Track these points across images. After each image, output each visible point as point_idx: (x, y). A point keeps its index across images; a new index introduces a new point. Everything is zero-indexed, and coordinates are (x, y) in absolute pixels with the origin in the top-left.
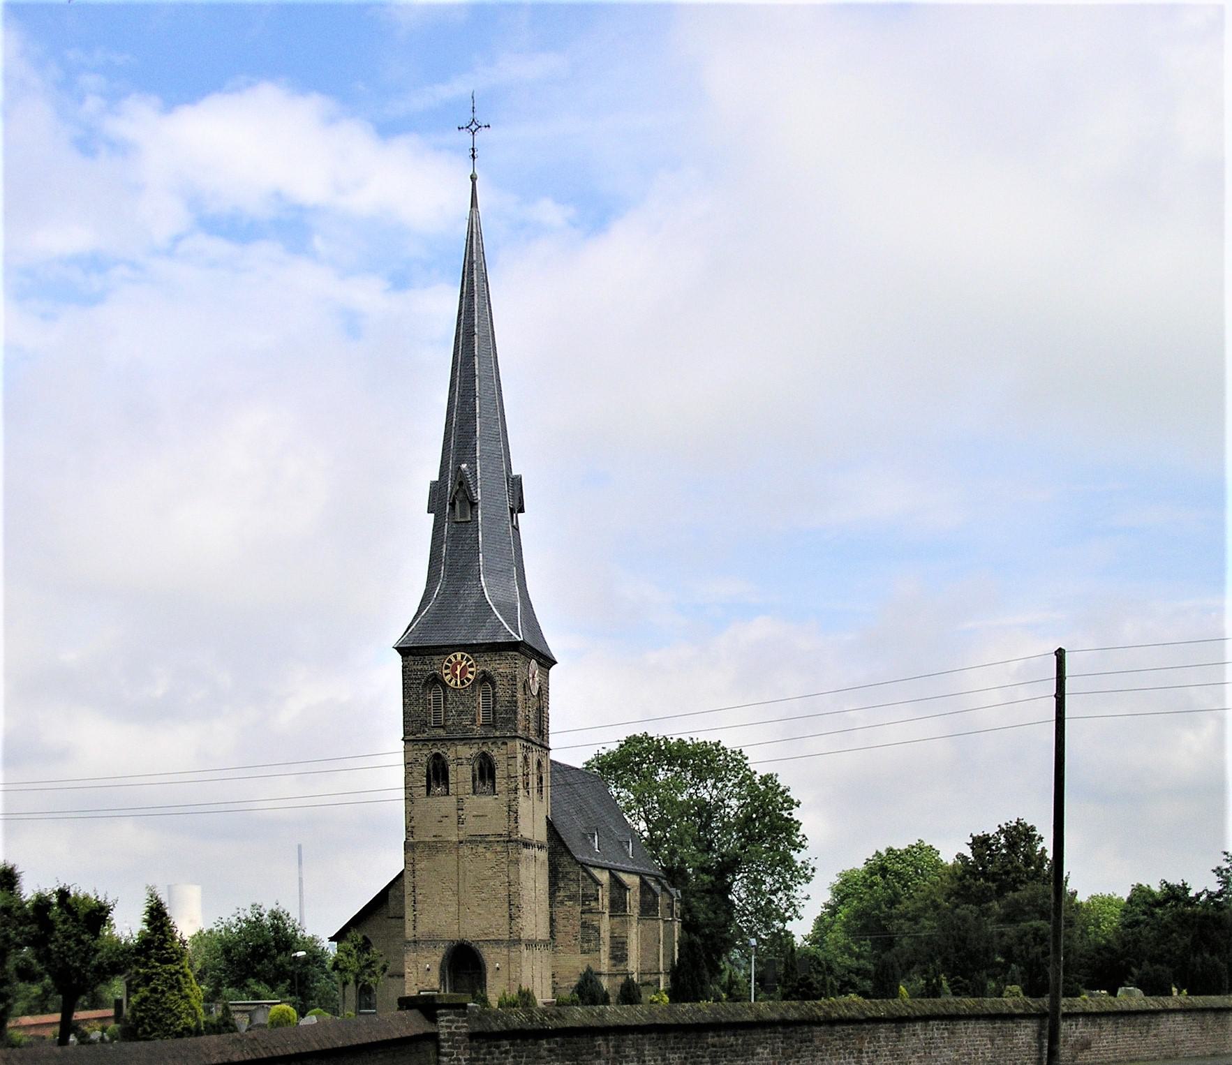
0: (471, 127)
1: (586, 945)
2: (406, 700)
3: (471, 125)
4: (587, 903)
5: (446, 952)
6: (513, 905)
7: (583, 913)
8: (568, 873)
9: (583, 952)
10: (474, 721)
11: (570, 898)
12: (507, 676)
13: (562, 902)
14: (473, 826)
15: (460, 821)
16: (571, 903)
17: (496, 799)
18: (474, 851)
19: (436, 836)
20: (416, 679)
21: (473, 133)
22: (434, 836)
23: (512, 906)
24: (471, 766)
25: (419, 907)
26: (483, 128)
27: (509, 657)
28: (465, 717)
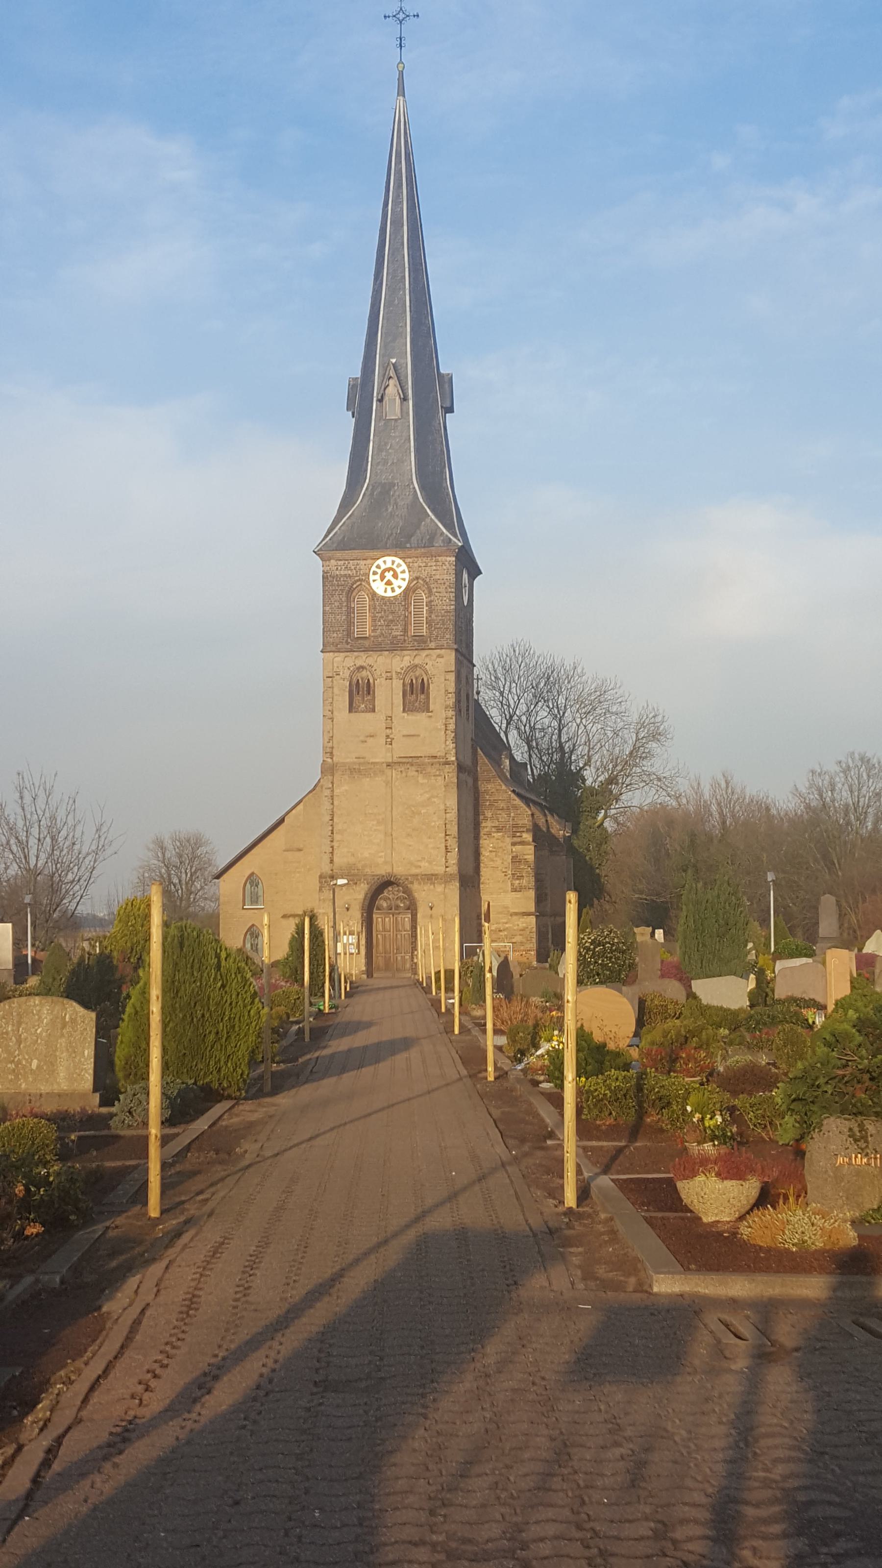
0: (404, 16)
1: (518, 882)
2: (327, 608)
3: (398, 13)
4: (518, 834)
5: (369, 890)
6: (448, 835)
7: (513, 844)
8: (496, 801)
9: (514, 890)
10: (405, 630)
11: (499, 829)
12: (444, 583)
13: (489, 834)
14: (401, 749)
15: (389, 740)
16: (499, 834)
17: (430, 717)
18: (404, 774)
19: (359, 758)
20: (338, 585)
21: (401, 22)
22: (356, 758)
23: (447, 837)
24: (402, 681)
25: (337, 837)
26: (391, 15)
27: (447, 563)
28: (394, 628)
